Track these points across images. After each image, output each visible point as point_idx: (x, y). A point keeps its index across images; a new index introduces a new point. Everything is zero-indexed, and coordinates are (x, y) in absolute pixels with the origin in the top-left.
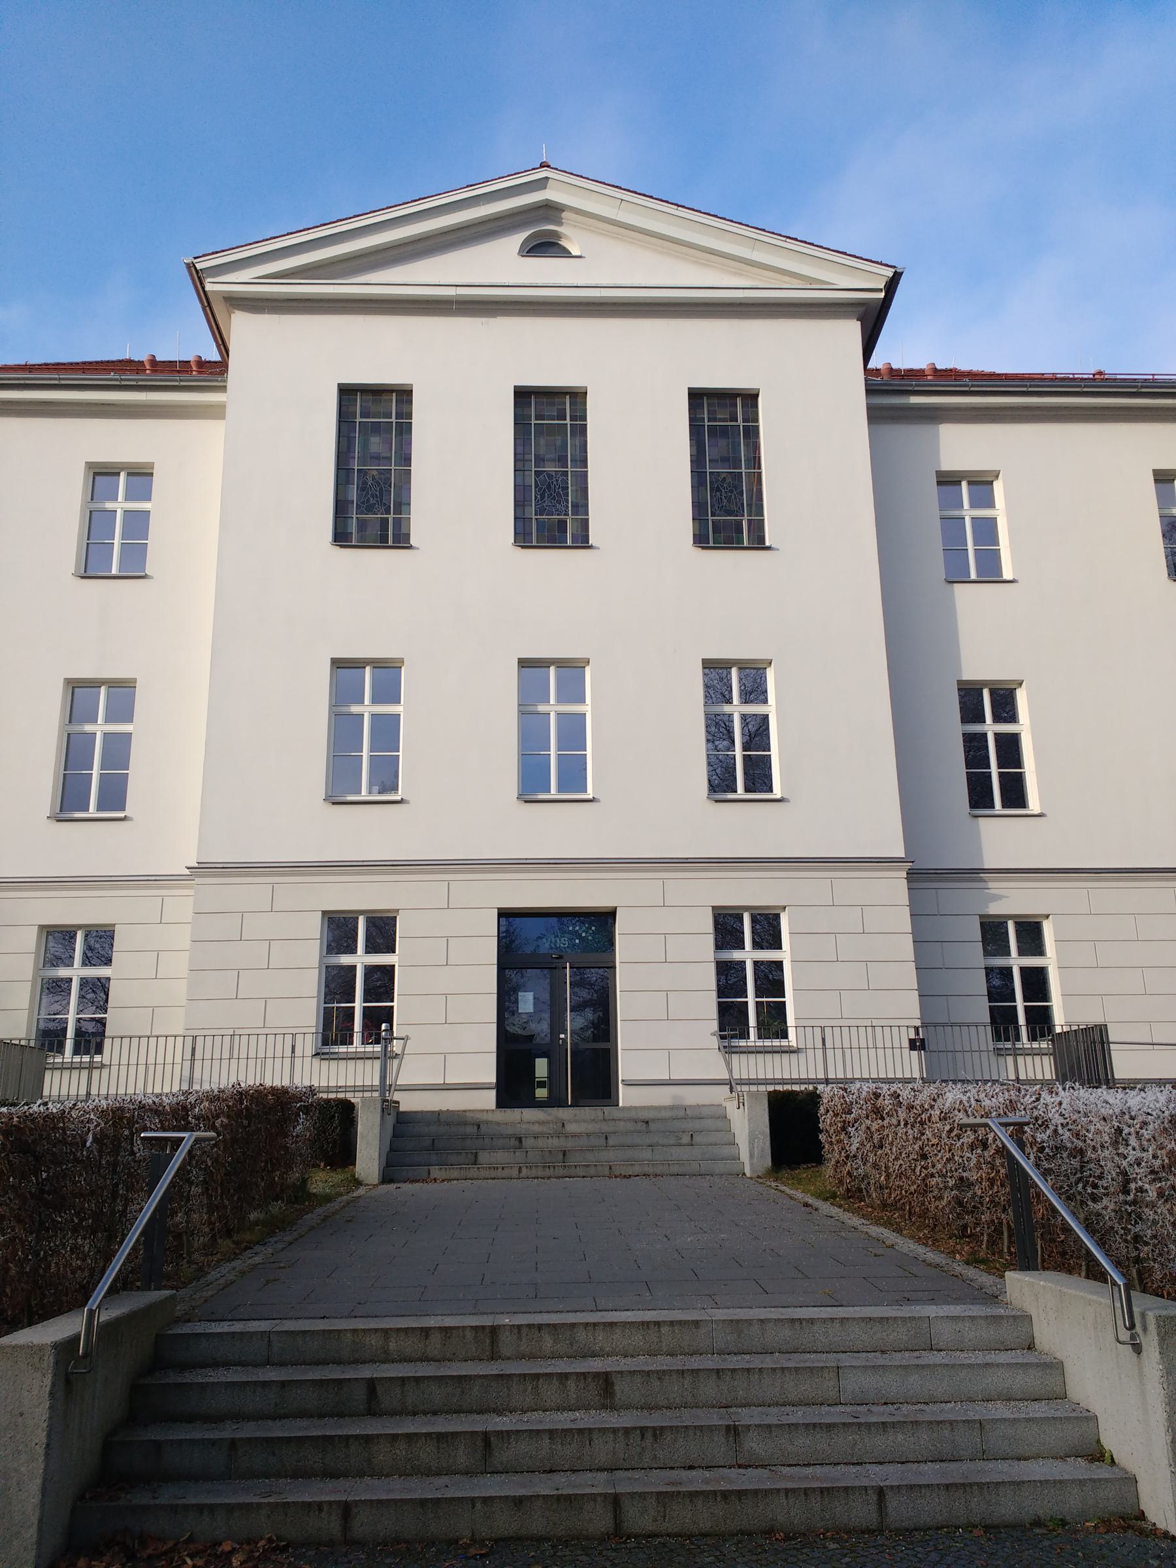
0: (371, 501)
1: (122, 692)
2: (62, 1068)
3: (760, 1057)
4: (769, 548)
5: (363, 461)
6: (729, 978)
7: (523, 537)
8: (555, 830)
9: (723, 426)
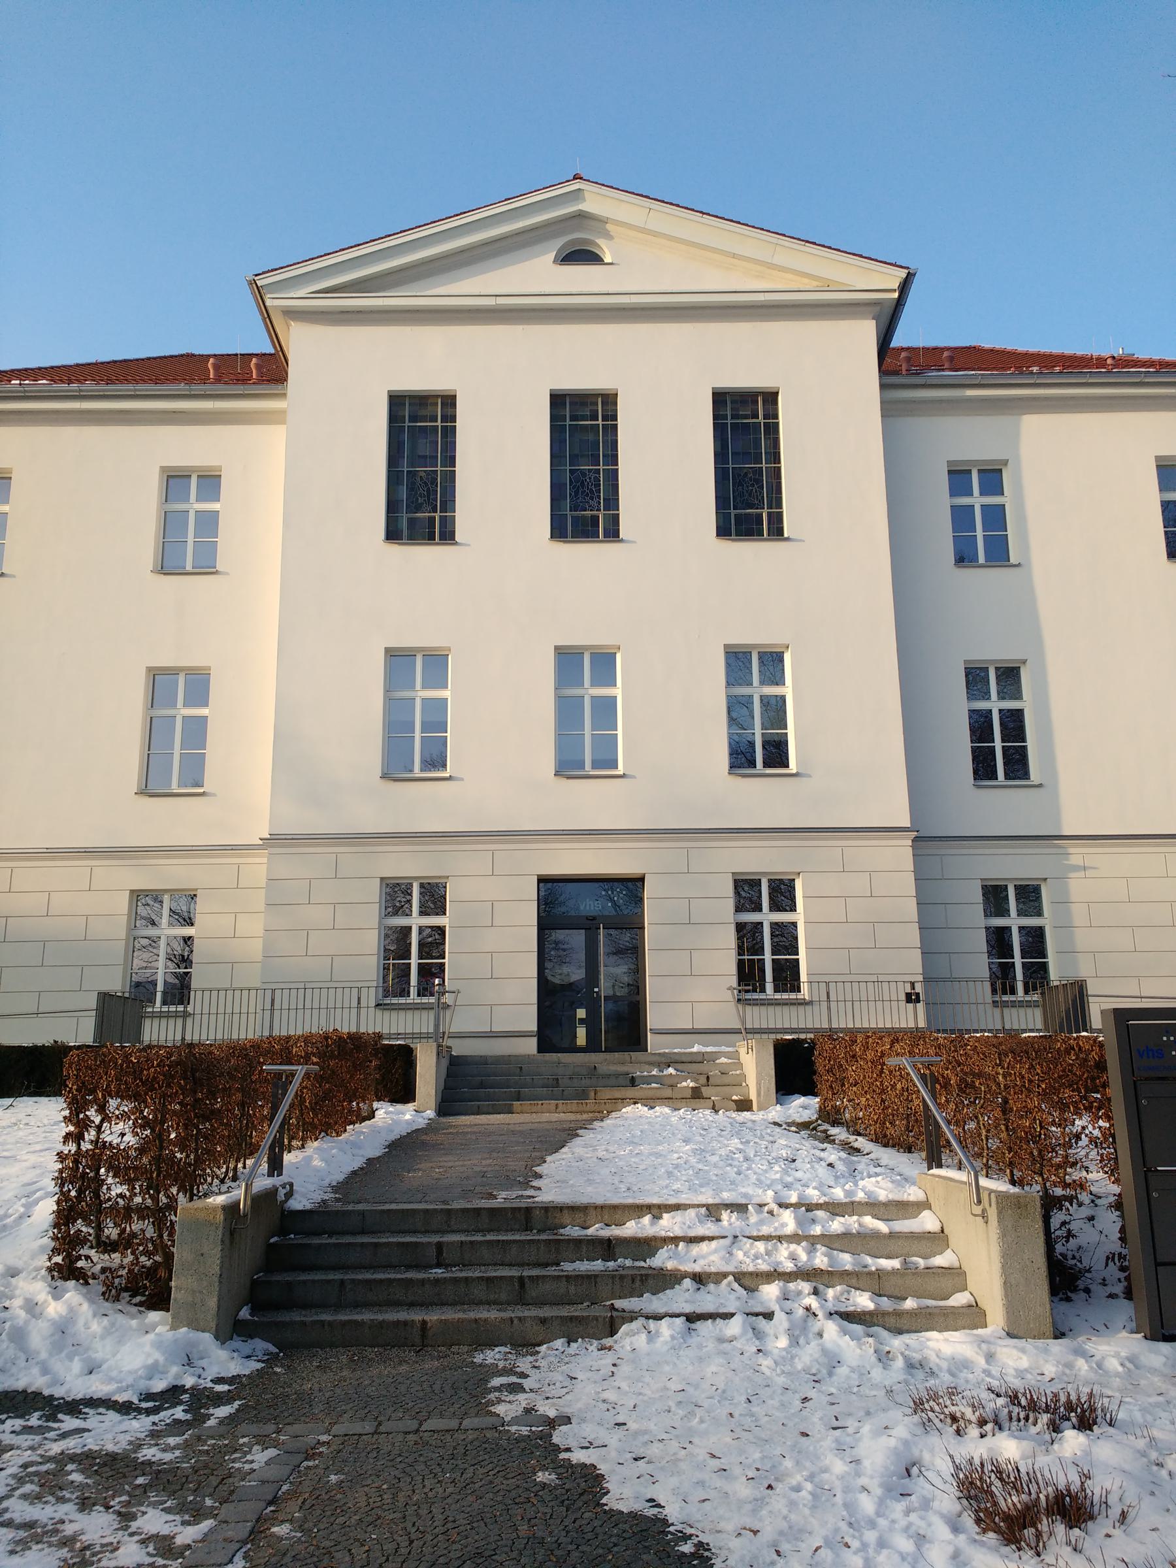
0: (420, 490)
1: (198, 684)
2: (153, 1016)
3: (786, 1008)
4: (788, 539)
5: (412, 464)
6: (748, 937)
7: (560, 531)
8: (593, 802)
9: (745, 432)
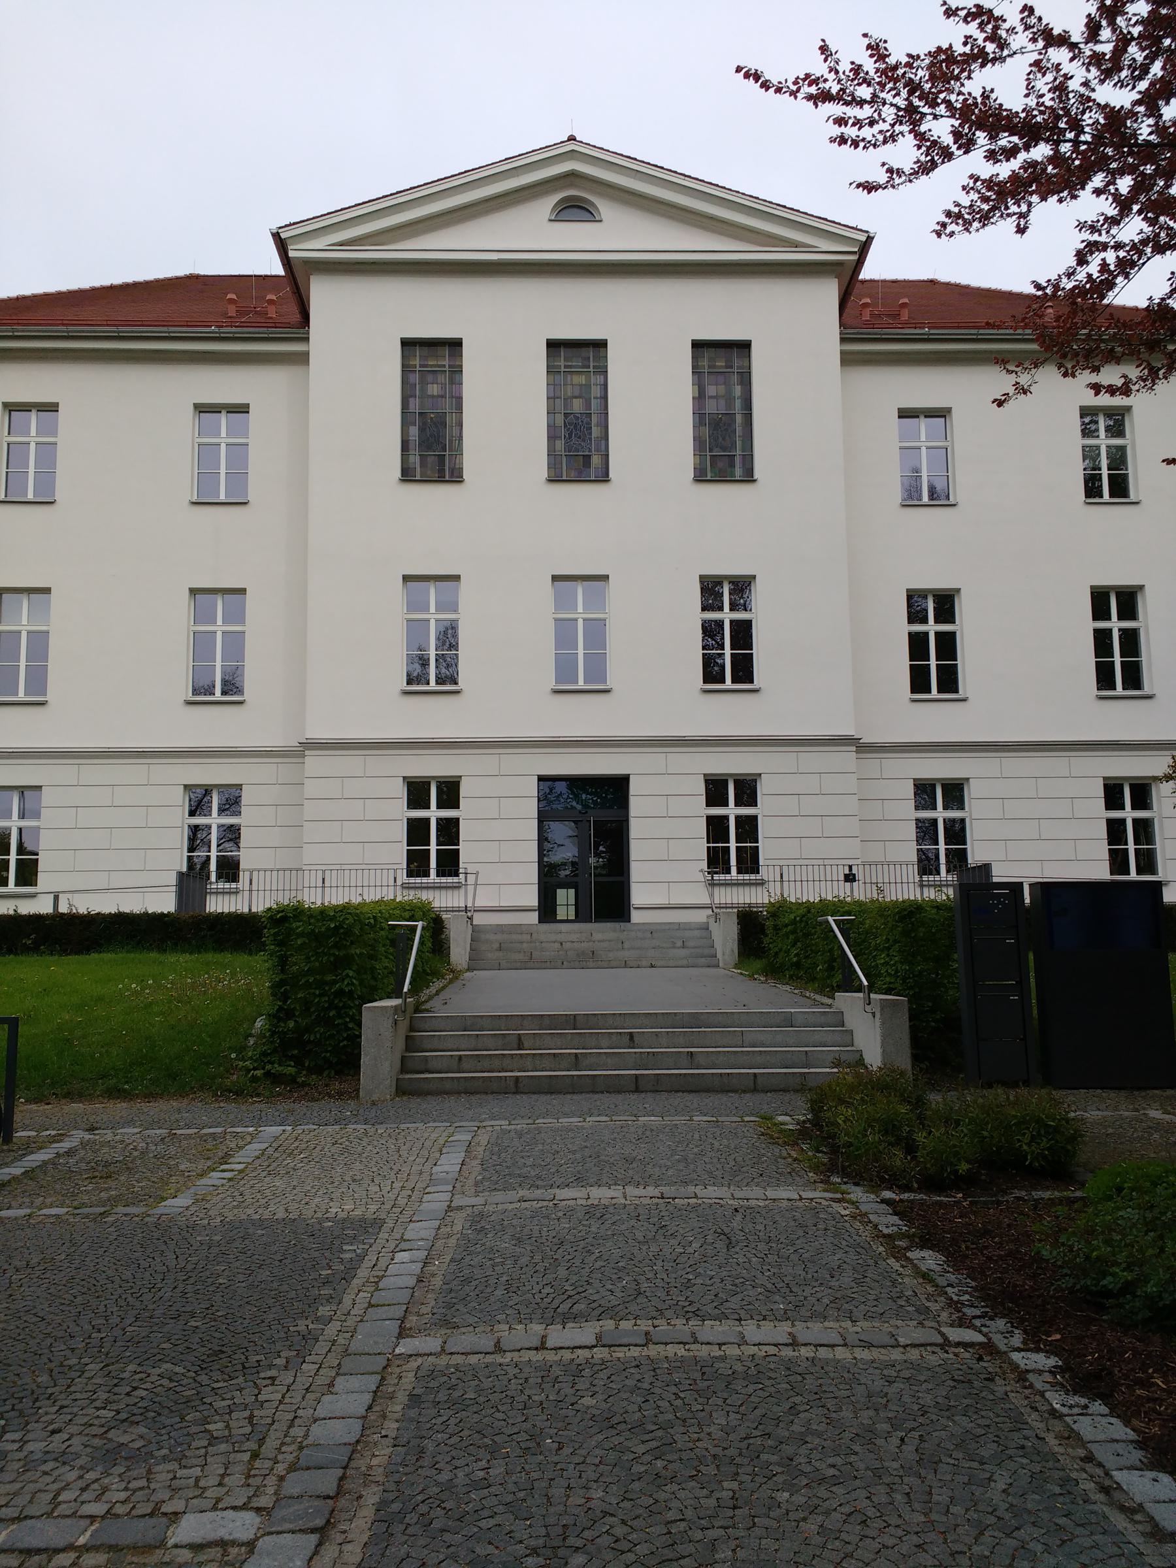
0: (432, 449)
